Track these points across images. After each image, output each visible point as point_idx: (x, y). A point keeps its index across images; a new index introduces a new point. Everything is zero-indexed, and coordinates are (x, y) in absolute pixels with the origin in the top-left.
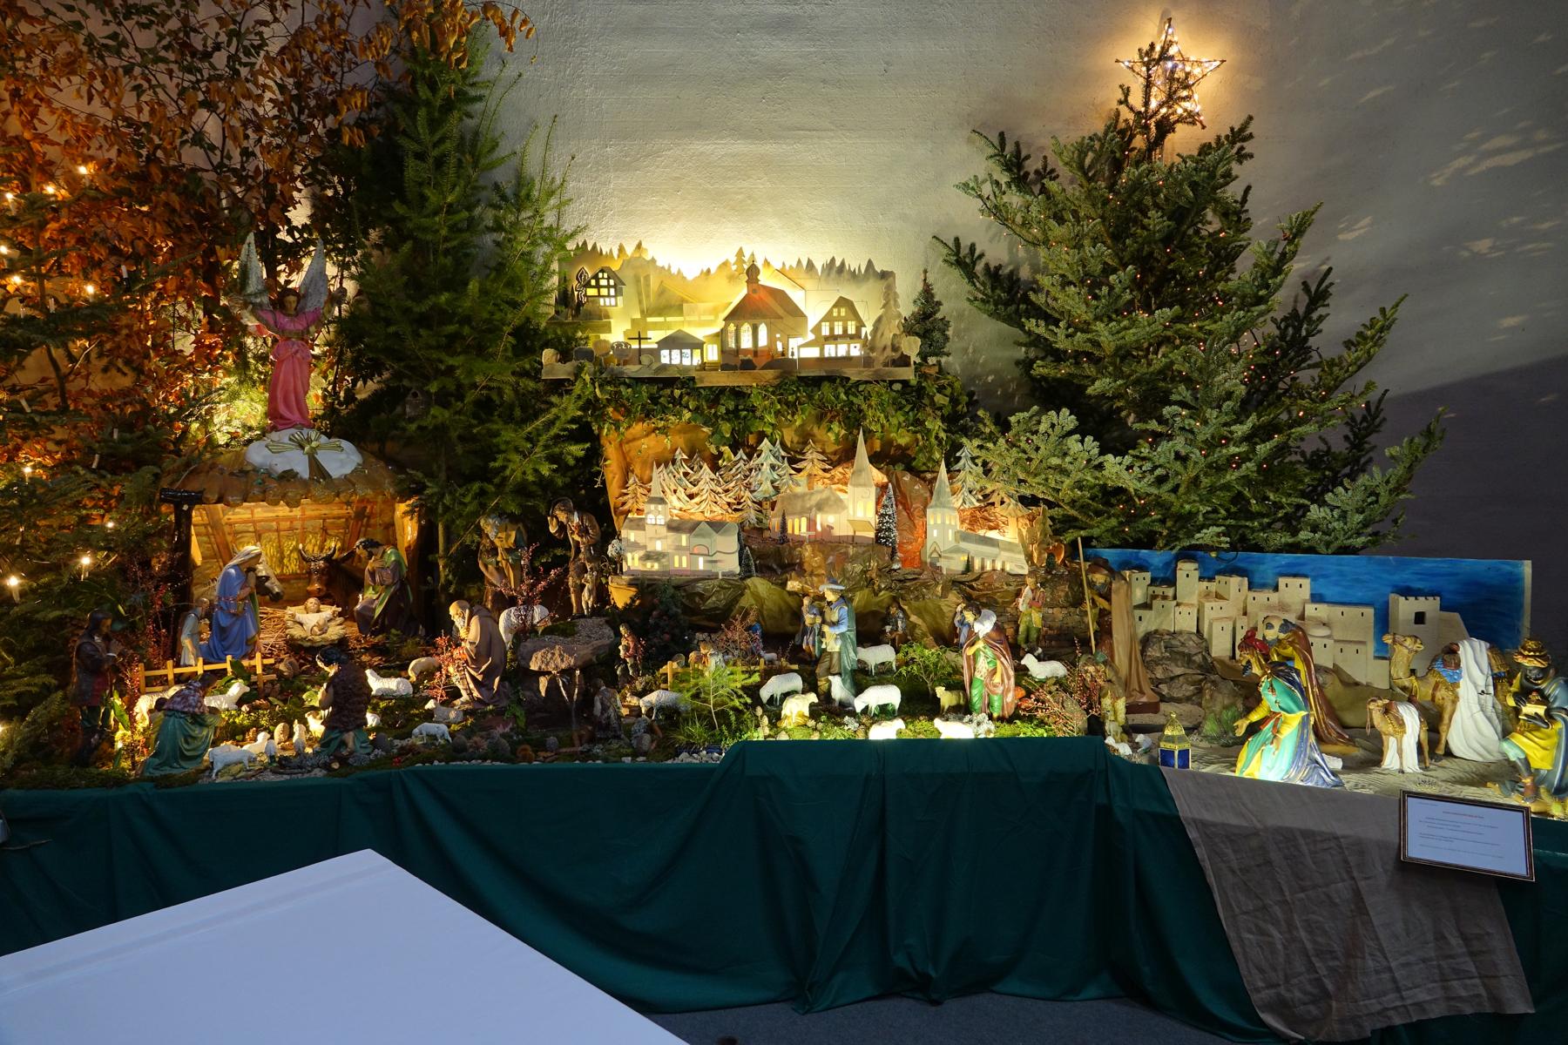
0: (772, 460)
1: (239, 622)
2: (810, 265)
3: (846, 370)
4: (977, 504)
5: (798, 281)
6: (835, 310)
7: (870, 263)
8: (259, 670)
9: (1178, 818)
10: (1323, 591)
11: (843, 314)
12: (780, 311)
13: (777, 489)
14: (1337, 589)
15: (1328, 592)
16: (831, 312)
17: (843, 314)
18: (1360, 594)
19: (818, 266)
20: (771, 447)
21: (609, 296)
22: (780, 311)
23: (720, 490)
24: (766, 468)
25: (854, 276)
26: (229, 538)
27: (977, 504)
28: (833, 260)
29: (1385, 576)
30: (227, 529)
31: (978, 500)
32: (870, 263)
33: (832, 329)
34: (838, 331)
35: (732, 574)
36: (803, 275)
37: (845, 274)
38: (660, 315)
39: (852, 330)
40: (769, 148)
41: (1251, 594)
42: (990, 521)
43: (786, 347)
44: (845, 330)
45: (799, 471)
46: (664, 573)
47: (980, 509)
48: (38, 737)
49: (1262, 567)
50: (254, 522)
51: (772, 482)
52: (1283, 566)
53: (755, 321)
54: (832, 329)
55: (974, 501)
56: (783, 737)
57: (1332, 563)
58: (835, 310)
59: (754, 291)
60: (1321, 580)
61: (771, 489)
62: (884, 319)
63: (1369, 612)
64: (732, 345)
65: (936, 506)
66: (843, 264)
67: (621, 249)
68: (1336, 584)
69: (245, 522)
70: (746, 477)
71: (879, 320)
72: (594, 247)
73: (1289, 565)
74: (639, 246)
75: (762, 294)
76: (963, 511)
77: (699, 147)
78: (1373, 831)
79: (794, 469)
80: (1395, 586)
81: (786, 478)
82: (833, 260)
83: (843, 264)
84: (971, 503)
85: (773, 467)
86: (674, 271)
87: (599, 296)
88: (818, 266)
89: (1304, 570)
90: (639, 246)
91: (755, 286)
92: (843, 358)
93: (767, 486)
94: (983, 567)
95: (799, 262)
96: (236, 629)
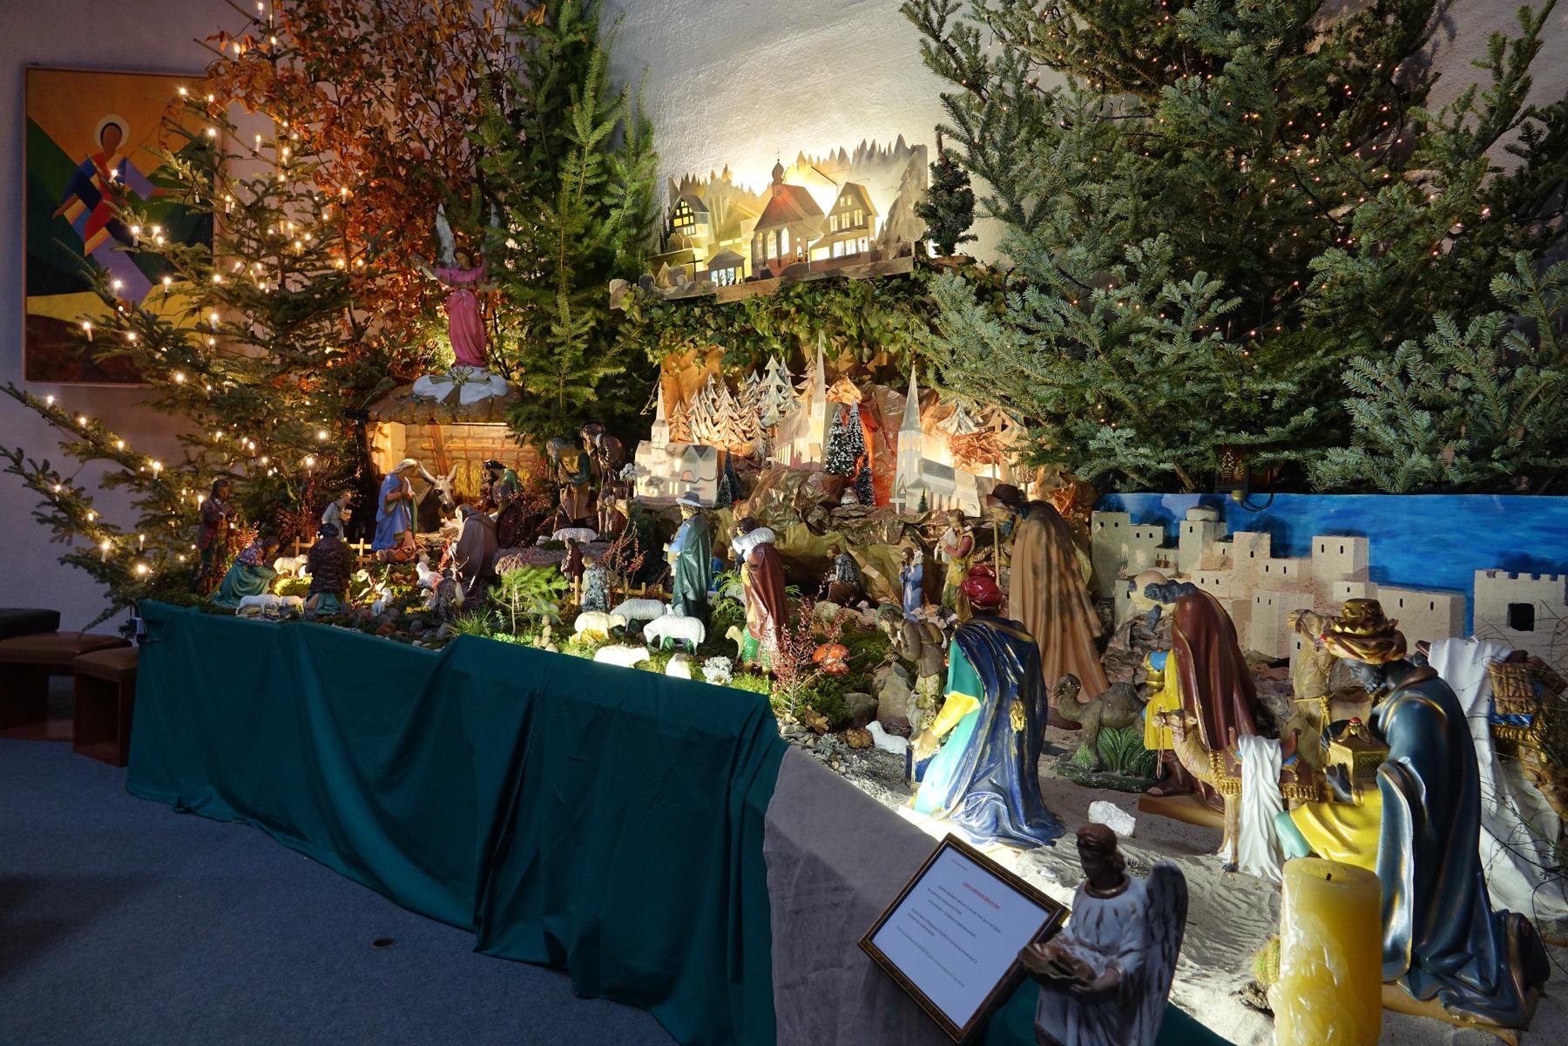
0: (778, 381)
1: (389, 519)
2: (842, 153)
3: (843, 269)
4: (976, 430)
5: (830, 176)
6: (842, 200)
7: (900, 139)
8: (361, 553)
9: (763, 818)
10: (1385, 562)
11: (849, 203)
12: (800, 211)
13: (782, 412)
14: (1409, 559)
15: (1397, 564)
16: (838, 202)
17: (849, 203)
18: (1443, 569)
19: (850, 155)
20: (777, 366)
21: (690, 224)
22: (800, 211)
23: (736, 417)
24: (773, 390)
25: (884, 157)
26: (448, 462)
27: (976, 430)
28: (864, 143)
29: (1484, 534)
30: (447, 454)
31: (977, 424)
32: (900, 139)
33: (840, 223)
34: (846, 224)
35: (710, 502)
36: (835, 168)
37: (875, 159)
38: (729, 238)
39: (859, 221)
40: (827, 34)
41: (1279, 564)
42: (988, 451)
43: (805, 251)
44: (852, 223)
45: (800, 392)
46: (661, 499)
47: (978, 436)
48: (1549, 870)
49: (1304, 519)
50: (466, 451)
51: (778, 406)
52: (1331, 517)
53: (778, 227)
54: (840, 223)
55: (971, 424)
56: (572, 649)
57: (1402, 510)
58: (842, 200)
59: (779, 193)
60: (1385, 541)
61: (777, 414)
62: (900, 204)
63: (1443, 600)
64: (761, 257)
65: (906, 428)
66: (873, 146)
67: (713, 176)
68: (1407, 550)
69: (459, 450)
70: (758, 400)
71: (895, 206)
72: (694, 178)
73: (1340, 515)
74: (726, 170)
75: (785, 195)
76: (958, 438)
77: (768, 51)
78: (867, 885)
79: (797, 390)
80: (1502, 555)
81: (789, 400)
82: (864, 143)
83: (873, 146)
84: (968, 428)
85: (779, 389)
86: (746, 189)
87: (683, 226)
88: (850, 155)
89: (1362, 523)
90: (726, 170)
91: (779, 187)
92: (840, 259)
93: (774, 411)
94: (940, 507)
95: (832, 153)
96: (387, 524)
